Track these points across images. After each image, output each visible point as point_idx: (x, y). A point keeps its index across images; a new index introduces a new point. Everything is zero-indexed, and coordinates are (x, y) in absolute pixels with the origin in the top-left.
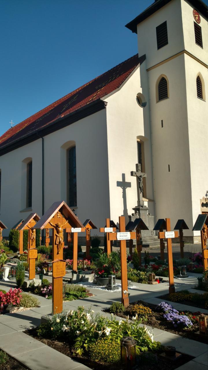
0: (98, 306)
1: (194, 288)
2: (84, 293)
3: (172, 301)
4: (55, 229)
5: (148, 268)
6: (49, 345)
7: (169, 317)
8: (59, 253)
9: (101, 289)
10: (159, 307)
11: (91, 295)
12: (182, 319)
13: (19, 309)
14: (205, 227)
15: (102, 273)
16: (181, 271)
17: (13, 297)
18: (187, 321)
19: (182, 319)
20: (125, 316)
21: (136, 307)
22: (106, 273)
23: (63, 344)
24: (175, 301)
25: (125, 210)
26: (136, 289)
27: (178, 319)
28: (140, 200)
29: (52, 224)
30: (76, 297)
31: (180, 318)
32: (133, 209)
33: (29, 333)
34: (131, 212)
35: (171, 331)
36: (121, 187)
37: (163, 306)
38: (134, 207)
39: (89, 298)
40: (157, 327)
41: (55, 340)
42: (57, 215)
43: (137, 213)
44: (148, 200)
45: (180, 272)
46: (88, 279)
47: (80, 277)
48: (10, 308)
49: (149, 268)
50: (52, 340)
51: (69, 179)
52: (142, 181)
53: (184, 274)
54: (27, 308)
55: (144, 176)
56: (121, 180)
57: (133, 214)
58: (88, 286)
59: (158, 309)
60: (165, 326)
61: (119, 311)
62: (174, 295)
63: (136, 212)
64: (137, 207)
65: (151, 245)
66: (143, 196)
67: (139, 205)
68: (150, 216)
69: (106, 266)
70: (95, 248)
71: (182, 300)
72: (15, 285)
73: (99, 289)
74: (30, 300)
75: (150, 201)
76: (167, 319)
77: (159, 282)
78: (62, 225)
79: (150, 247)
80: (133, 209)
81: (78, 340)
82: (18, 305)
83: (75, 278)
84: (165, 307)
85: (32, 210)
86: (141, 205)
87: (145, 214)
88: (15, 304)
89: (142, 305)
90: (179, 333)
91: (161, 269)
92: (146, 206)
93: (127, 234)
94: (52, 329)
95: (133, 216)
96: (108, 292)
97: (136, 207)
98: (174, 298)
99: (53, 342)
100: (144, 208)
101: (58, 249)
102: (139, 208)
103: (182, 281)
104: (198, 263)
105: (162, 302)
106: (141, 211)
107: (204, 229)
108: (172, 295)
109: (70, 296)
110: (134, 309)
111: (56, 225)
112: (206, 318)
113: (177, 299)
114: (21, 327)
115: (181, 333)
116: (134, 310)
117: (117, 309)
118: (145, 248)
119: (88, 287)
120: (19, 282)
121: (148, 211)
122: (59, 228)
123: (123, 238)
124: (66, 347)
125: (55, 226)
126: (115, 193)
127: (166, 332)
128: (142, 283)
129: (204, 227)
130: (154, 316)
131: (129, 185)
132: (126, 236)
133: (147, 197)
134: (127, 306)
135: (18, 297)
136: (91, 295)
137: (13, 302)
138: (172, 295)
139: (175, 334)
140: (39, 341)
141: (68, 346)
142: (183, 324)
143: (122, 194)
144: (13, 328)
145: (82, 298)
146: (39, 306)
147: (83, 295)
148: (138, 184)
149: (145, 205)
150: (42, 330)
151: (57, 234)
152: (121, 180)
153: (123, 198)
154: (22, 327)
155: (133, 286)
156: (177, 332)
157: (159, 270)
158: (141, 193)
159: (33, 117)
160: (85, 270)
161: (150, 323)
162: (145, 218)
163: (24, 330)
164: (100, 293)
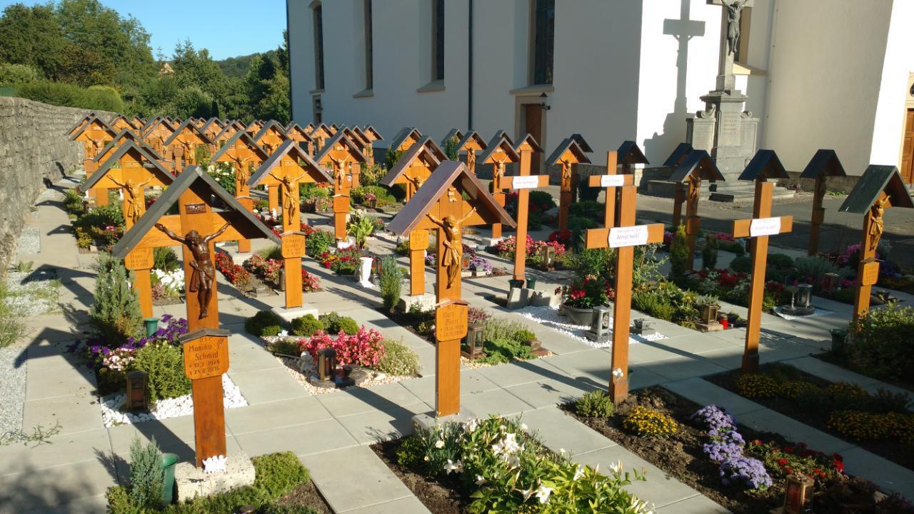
0: (554, 390)
1: (816, 356)
2: (527, 348)
3: (743, 396)
4: (441, 229)
5: (709, 280)
6: (417, 493)
7: (717, 453)
8: (452, 285)
9: (574, 336)
10: (698, 416)
11: (542, 351)
12: (744, 468)
13: (375, 379)
14: (881, 202)
15: (580, 298)
16: (793, 299)
17: (364, 349)
18: (757, 474)
19: (745, 471)
20: (611, 428)
21: (638, 412)
22: (588, 298)
23: (447, 495)
24: (752, 396)
25: (681, 101)
26: (664, 341)
27: (735, 467)
28: (726, 74)
29: (433, 218)
30: (507, 354)
31: (740, 466)
32: (703, 99)
33: (382, 451)
34: (695, 105)
35: (711, 492)
36: (675, 36)
37: (709, 417)
38: (706, 93)
39: (536, 362)
40: (679, 475)
41: (433, 481)
42: (448, 196)
43: (711, 110)
44: (748, 72)
45: (791, 300)
46: (548, 300)
47: (530, 295)
48: (358, 375)
49: (712, 280)
50: (426, 480)
51: (536, 9)
52: (737, 20)
53: (804, 305)
54: (393, 377)
55: (747, 5)
56: (677, 16)
57: (699, 114)
58: (545, 321)
59: (696, 419)
60: (701, 477)
61: (597, 415)
62: (749, 380)
63: (708, 108)
64: (714, 95)
65: (739, 196)
66: (736, 60)
67: (720, 88)
68: (748, 119)
69: (592, 280)
70: (587, 201)
71: (769, 396)
72: (380, 300)
73: (566, 332)
74: (400, 359)
75: (755, 72)
76: (712, 456)
77: (727, 326)
78: (462, 218)
79: (735, 200)
80: (703, 99)
81: (479, 498)
82: (375, 367)
83: (516, 296)
84: (714, 419)
85: (445, 88)
86: (726, 89)
87: (733, 112)
88: (368, 364)
89: (659, 402)
90: (732, 502)
91: (742, 287)
92: (740, 91)
93: (637, 230)
94: (426, 459)
95: (700, 119)
96: (590, 347)
97: (711, 92)
98: (749, 389)
99: (427, 486)
100: (733, 96)
101: (449, 276)
102: (719, 98)
103: (789, 326)
104: (853, 270)
105: (709, 407)
106: (723, 106)
107: (878, 205)
108: (745, 380)
109: (492, 352)
110: (632, 418)
111: (444, 219)
112: (805, 487)
113: (756, 391)
114: (370, 431)
115: (734, 503)
116: (632, 421)
117: (593, 408)
118: (721, 203)
119: (543, 323)
120: (389, 298)
121: (744, 103)
122: (451, 227)
123: (626, 243)
124: (452, 503)
125: (442, 222)
126: (656, 51)
127: (699, 493)
128: (680, 325)
129: (878, 202)
130: (680, 440)
131: (699, 28)
132: (636, 236)
133: (749, 62)
134: (622, 400)
135: (377, 349)
136: (542, 351)
137: (365, 359)
138: (746, 376)
139: (720, 502)
140: (398, 478)
141: (458, 502)
142: (745, 482)
143: (677, 54)
144: (352, 433)
145: (521, 360)
146: (420, 373)
147: (525, 353)
148: (726, 29)
149: (737, 88)
150: (407, 453)
151: (447, 242)
152: (677, 16)
153: (677, 65)
154: (371, 434)
155: (654, 333)
156: (726, 497)
157: (737, 287)
158: (729, 54)
159: (315, 23)
160: (549, 269)
161: (664, 461)
162: (734, 128)
163: (374, 442)
164: (570, 350)
